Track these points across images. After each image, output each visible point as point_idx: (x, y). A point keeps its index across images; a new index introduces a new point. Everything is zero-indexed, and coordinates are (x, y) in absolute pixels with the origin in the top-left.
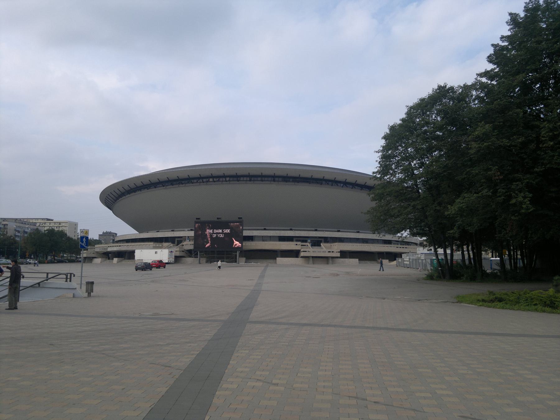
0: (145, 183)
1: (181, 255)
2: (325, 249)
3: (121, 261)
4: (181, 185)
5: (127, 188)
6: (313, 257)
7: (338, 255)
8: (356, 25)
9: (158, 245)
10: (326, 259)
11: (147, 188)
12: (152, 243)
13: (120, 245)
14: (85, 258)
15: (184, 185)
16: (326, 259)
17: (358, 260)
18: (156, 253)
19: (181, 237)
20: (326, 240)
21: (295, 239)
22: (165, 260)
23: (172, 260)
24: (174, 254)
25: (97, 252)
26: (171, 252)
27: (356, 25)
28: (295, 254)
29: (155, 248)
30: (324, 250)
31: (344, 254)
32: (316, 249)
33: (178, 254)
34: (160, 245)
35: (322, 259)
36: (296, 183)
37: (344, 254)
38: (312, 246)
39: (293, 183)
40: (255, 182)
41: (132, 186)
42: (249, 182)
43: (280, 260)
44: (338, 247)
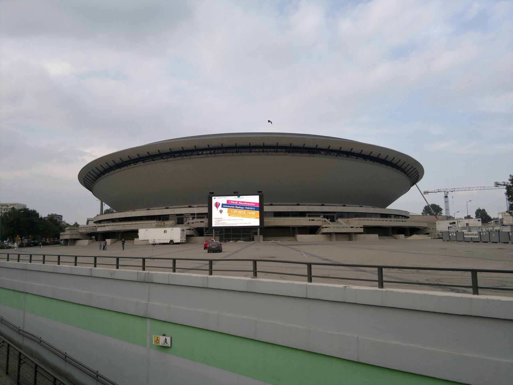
0: (151, 154)
1: (191, 234)
2: (345, 225)
3: (115, 242)
4: (185, 157)
5: (106, 166)
6: (336, 233)
7: (362, 230)
8: (309, 20)
9: (161, 223)
10: (349, 236)
11: (134, 163)
12: (155, 221)
13: (104, 225)
14: (66, 241)
15: (188, 157)
16: (349, 236)
17: (377, 235)
18: (165, 232)
19: (182, 215)
20: (342, 215)
21: (307, 214)
22: (177, 239)
23: (184, 239)
24: (185, 233)
25: (82, 234)
26: (183, 230)
27: (309, 20)
28: (313, 230)
29: (158, 226)
30: (343, 225)
31: (369, 230)
32: (332, 225)
33: (189, 234)
34: (162, 224)
35: (343, 235)
36: (312, 155)
37: (369, 230)
38: (441, 209)
39: (308, 155)
40: (269, 153)
41: (118, 161)
42: (262, 153)
43: (300, 237)
44: (357, 224)
